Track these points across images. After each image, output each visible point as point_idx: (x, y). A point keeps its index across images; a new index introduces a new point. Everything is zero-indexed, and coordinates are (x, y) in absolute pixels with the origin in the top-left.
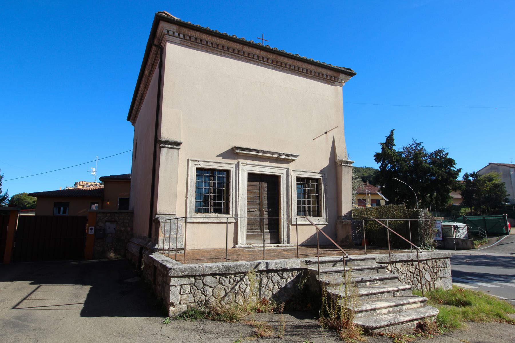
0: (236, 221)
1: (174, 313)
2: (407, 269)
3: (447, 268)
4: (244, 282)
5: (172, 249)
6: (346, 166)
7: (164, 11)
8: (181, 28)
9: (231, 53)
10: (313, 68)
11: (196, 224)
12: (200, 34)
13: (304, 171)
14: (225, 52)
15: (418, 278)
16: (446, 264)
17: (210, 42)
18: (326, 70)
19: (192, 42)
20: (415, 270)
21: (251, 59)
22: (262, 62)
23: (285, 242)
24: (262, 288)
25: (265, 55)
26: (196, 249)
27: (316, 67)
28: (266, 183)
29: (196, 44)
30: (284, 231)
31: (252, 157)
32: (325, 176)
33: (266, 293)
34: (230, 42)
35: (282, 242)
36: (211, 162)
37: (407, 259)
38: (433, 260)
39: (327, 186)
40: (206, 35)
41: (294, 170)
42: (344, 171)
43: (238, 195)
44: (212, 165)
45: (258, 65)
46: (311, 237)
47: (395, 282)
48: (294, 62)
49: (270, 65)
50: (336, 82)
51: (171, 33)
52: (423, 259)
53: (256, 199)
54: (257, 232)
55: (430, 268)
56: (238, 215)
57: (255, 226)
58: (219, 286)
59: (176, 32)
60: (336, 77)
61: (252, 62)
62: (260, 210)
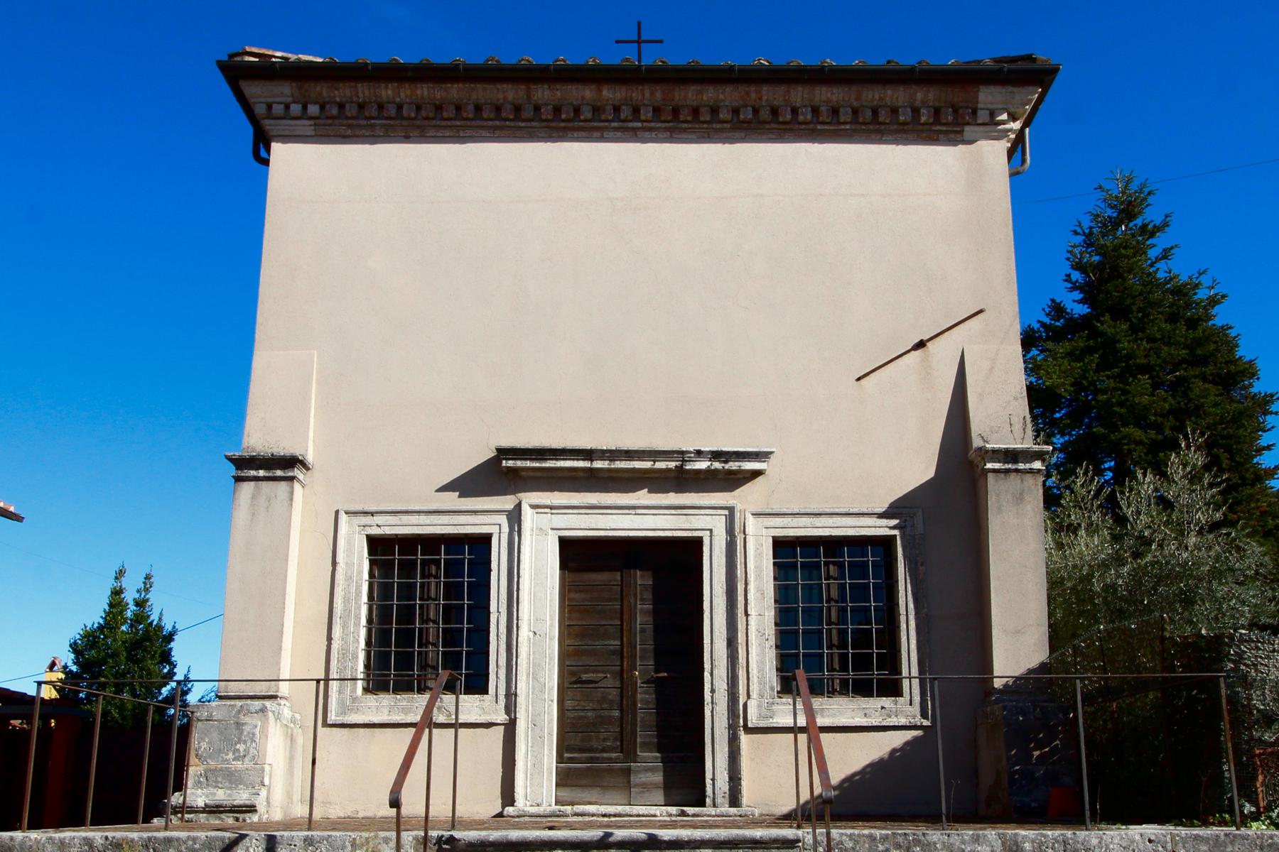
0: (510, 718)
6: (1007, 471)
7: (245, 49)
8: (306, 86)
9: (490, 123)
11: (362, 730)
12: (369, 89)
13: (808, 511)
14: (468, 123)
17: (409, 104)
19: (350, 122)
21: (570, 125)
22: (615, 124)
23: (719, 800)
25: (618, 95)
27: (854, 88)
28: (650, 573)
32: (913, 526)
35: (708, 801)
36: (419, 512)
40: (390, 85)
41: (759, 510)
42: (998, 495)
43: (517, 624)
44: (422, 523)
48: (747, 93)
49: (650, 129)
50: (967, 128)
54: (610, 760)
56: (516, 695)
57: (602, 737)
59: (294, 102)
60: (961, 105)
62: (623, 677)
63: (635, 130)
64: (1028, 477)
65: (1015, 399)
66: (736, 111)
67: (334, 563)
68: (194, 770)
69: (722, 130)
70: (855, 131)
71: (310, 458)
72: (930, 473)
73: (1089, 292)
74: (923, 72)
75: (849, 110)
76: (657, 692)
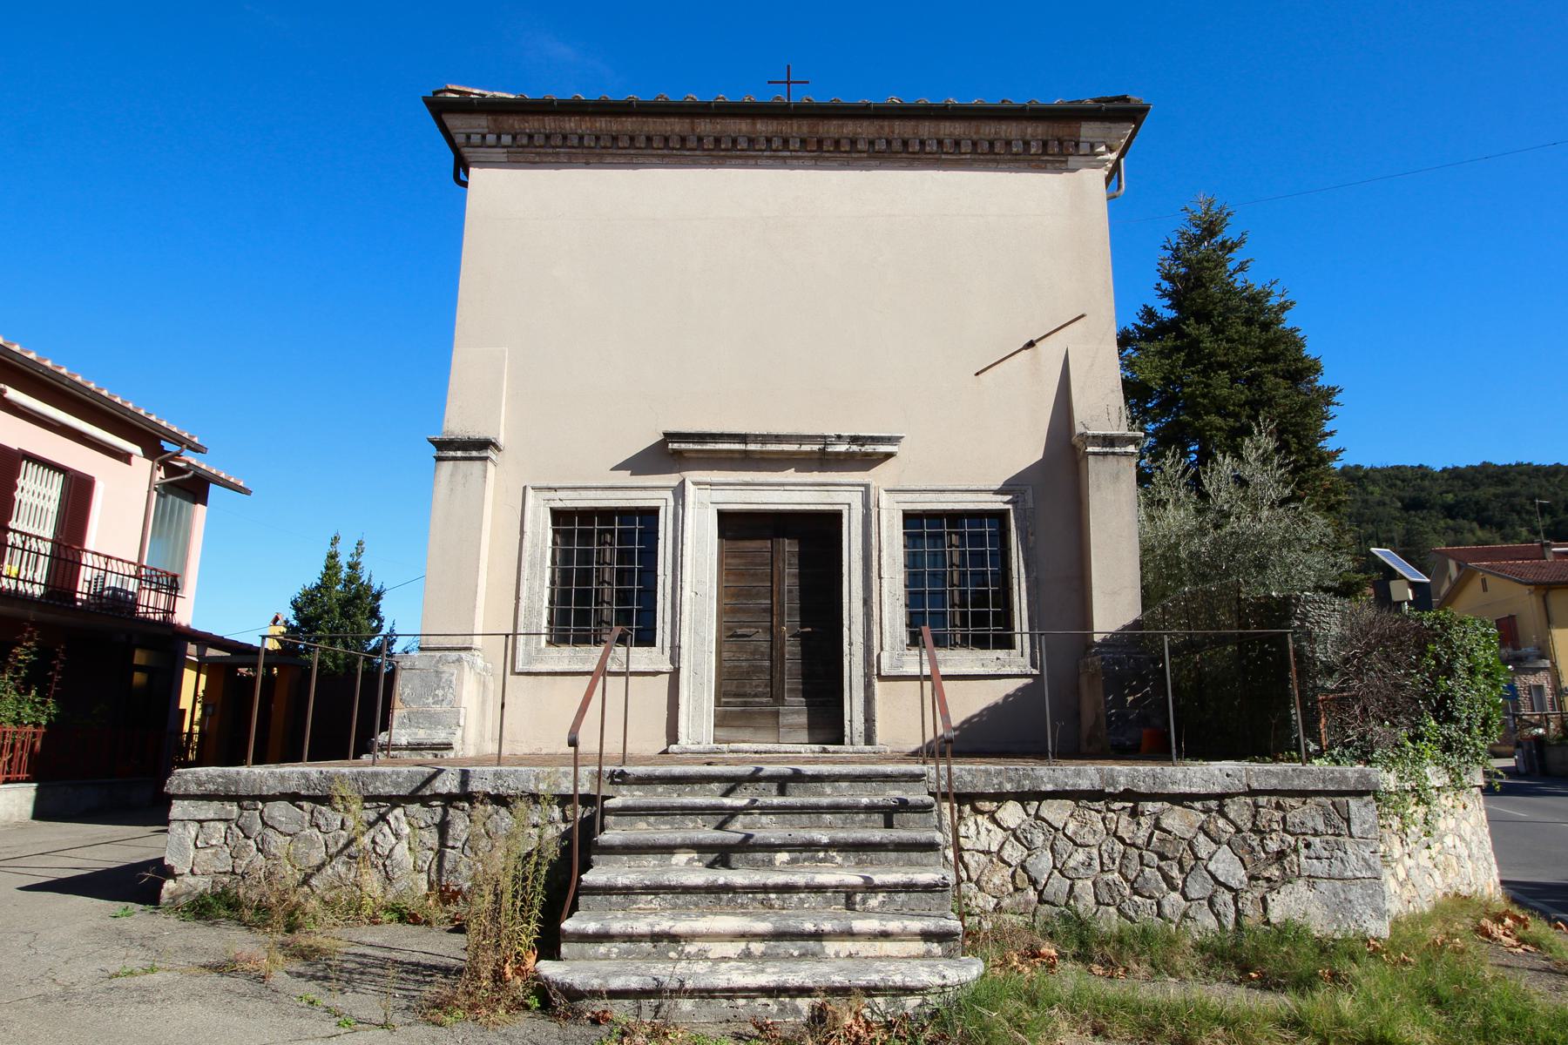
1: (174, 897)
2: (1101, 825)
3: (1351, 836)
4: (390, 827)
5: (418, 744)
6: (1105, 454)
8: (500, 118)
9: (659, 152)
10: (962, 130)
13: (934, 488)
14: (640, 152)
15: (1166, 868)
16: (1348, 820)
18: (1014, 124)
19: (538, 150)
20: (1152, 834)
21: (729, 153)
23: (856, 739)
24: (448, 850)
26: (544, 752)
27: (974, 123)
28: (796, 541)
29: (551, 151)
31: (732, 459)
33: (462, 867)
34: (650, 120)
36: (596, 488)
37: (1097, 788)
38: (1262, 800)
39: (1032, 534)
41: (891, 487)
42: (1097, 475)
45: (756, 166)
47: (925, 861)
48: (882, 127)
49: (798, 158)
50: (1070, 158)
51: (476, 139)
52: (1194, 790)
53: (758, 596)
54: (761, 704)
55: (1239, 830)
56: (680, 647)
58: (308, 831)
59: (490, 133)
60: (1067, 138)
63: (784, 158)
64: (1124, 459)
65: (1113, 391)
67: (522, 532)
68: (398, 713)
70: (974, 160)
71: (501, 441)
72: (1039, 456)
73: (1177, 300)
75: (970, 142)
76: (802, 645)
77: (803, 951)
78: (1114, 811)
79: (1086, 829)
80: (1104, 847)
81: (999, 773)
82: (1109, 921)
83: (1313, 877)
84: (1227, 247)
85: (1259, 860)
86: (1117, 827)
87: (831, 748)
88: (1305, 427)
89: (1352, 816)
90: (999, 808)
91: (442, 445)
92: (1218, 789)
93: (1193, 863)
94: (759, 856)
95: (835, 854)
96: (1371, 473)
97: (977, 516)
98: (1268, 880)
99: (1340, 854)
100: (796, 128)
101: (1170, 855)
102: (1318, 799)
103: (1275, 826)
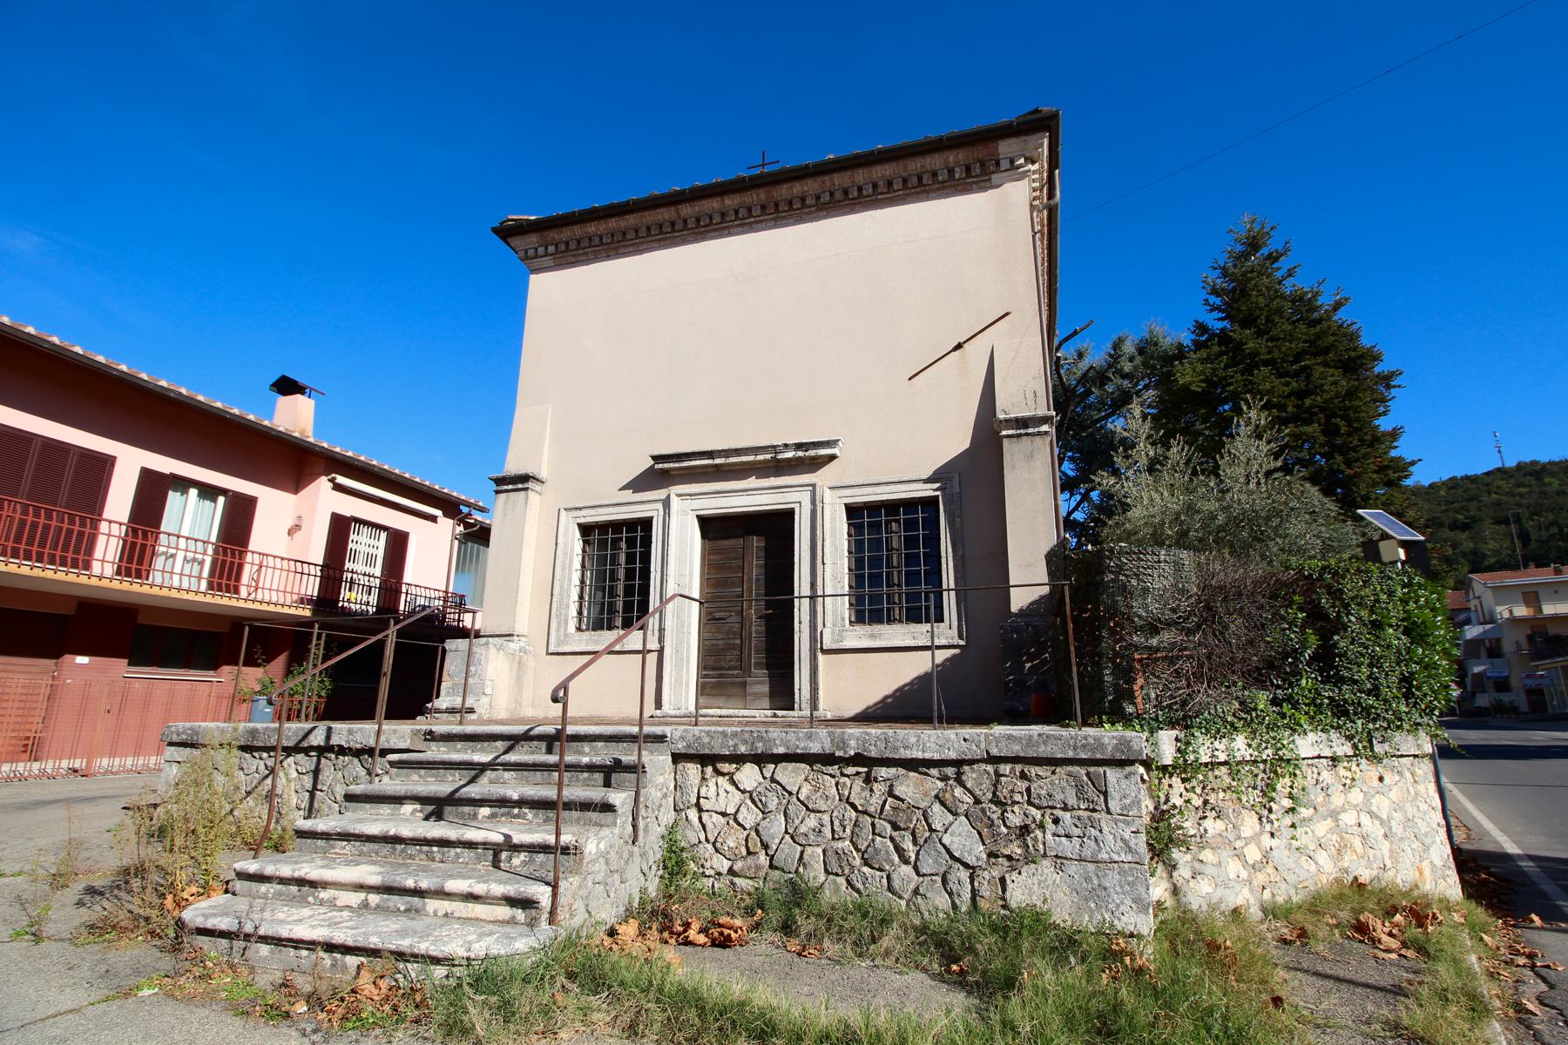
3: (1108, 812)
6: (1019, 436)
9: (657, 237)
15: (898, 839)
16: (1105, 794)
22: (736, 223)
23: (803, 706)
27: (900, 163)
28: (763, 538)
30: (803, 671)
31: (707, 473)
34: (646, 213)
35: (796, 706)
36: (608, 505)
37: (828, 751)
38: (1005, 768)
45: (730, 234)
46: (897, 690)
47: (603, 822)
48: (824, 182)
49: (761, 222)
50: (993, 176)
52: (928, 755)
53: (733, 585)
54: (732, 676)
55: (977, 801)
60: (987, 158)
61: (712, 234)
64: (1037, 439)
65: (1034, 378)
66: (818, 198)
69: (810, 213)
70: (907, 195)
71: (543, 474)
72: (966, 445)
73: (1229, 312)
74: (949, 139)
75: (900, 180)
76: (766, 625)
77: (408, 906)
78: (848, 776)
79: (819, 794)
80: (834, 814)
81: (735, 735)
82: (835, 892)
83: (1061, 857)
84: (1273, 258)
85: (999, 835)
86: (850, 793)
87: (780, 713)
88: (1356, 409)
89: (1110, 790)
90: (738, 769)
91: (499, 481)
92: (953, 755)
93: (927, 834)
94: (467, 809)
95: (527, 810)
96: (1548, 467)
97: (910, 504)
98: (1009, 858)
99: (1094, 832)
100: (755, 197)
101: (902, 825)
102: (1070, 768)
103: (1018, 797)
